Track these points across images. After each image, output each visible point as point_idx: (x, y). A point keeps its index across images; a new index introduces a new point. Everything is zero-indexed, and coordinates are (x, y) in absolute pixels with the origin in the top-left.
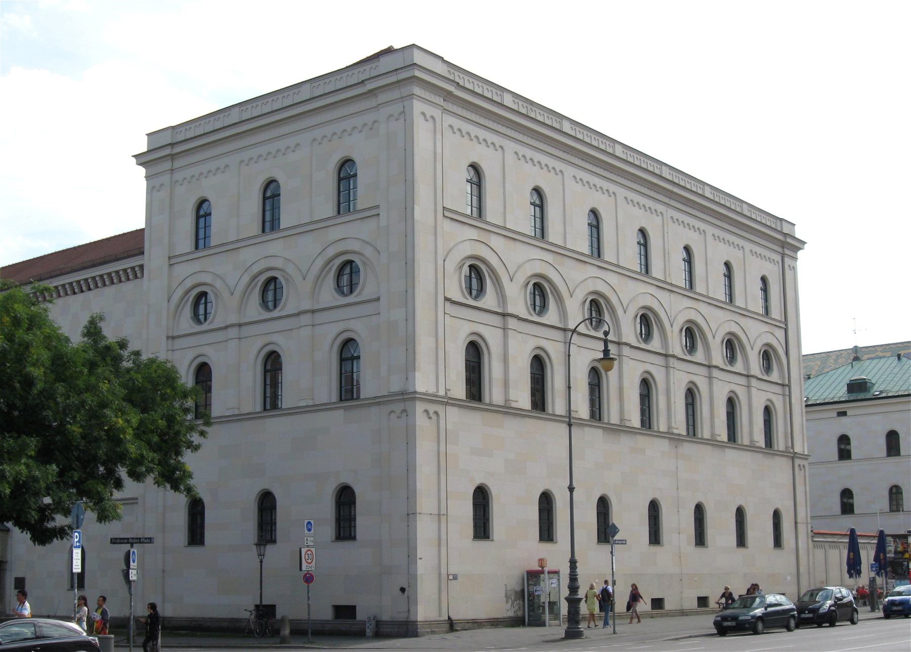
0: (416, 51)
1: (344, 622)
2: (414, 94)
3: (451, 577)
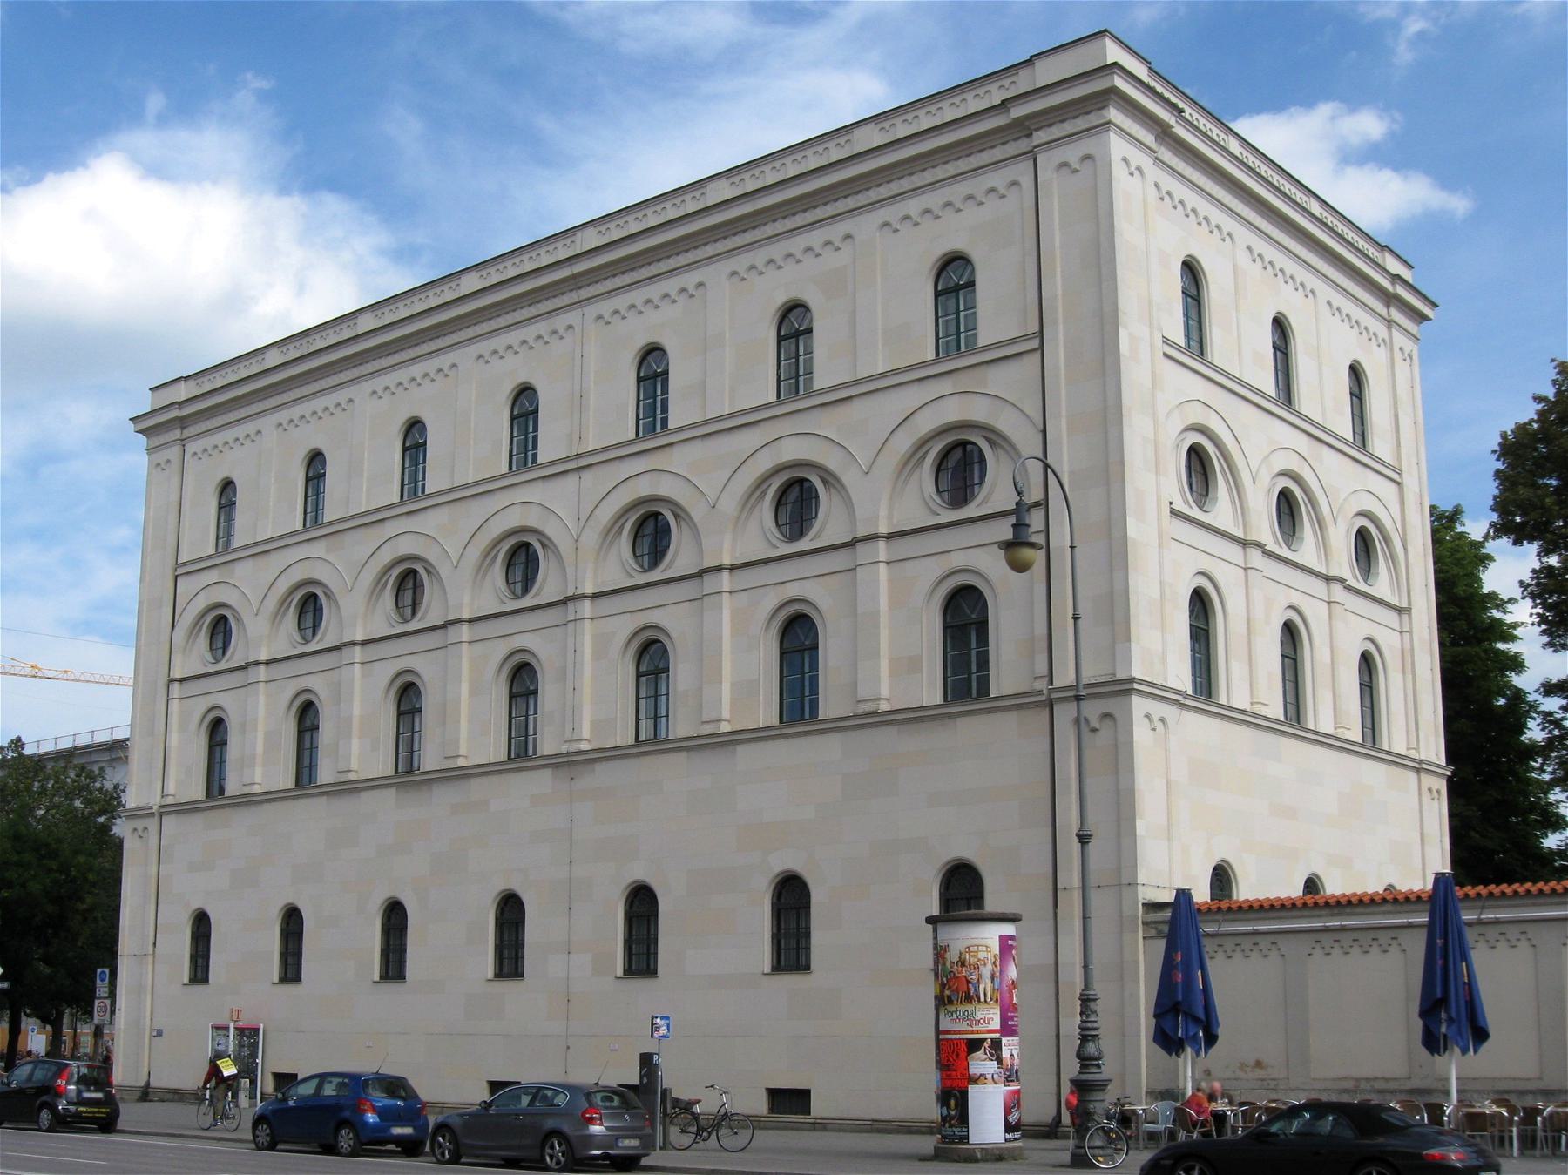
1: (802, 1120)
2: (1109, 122)
3: (155, 1033)
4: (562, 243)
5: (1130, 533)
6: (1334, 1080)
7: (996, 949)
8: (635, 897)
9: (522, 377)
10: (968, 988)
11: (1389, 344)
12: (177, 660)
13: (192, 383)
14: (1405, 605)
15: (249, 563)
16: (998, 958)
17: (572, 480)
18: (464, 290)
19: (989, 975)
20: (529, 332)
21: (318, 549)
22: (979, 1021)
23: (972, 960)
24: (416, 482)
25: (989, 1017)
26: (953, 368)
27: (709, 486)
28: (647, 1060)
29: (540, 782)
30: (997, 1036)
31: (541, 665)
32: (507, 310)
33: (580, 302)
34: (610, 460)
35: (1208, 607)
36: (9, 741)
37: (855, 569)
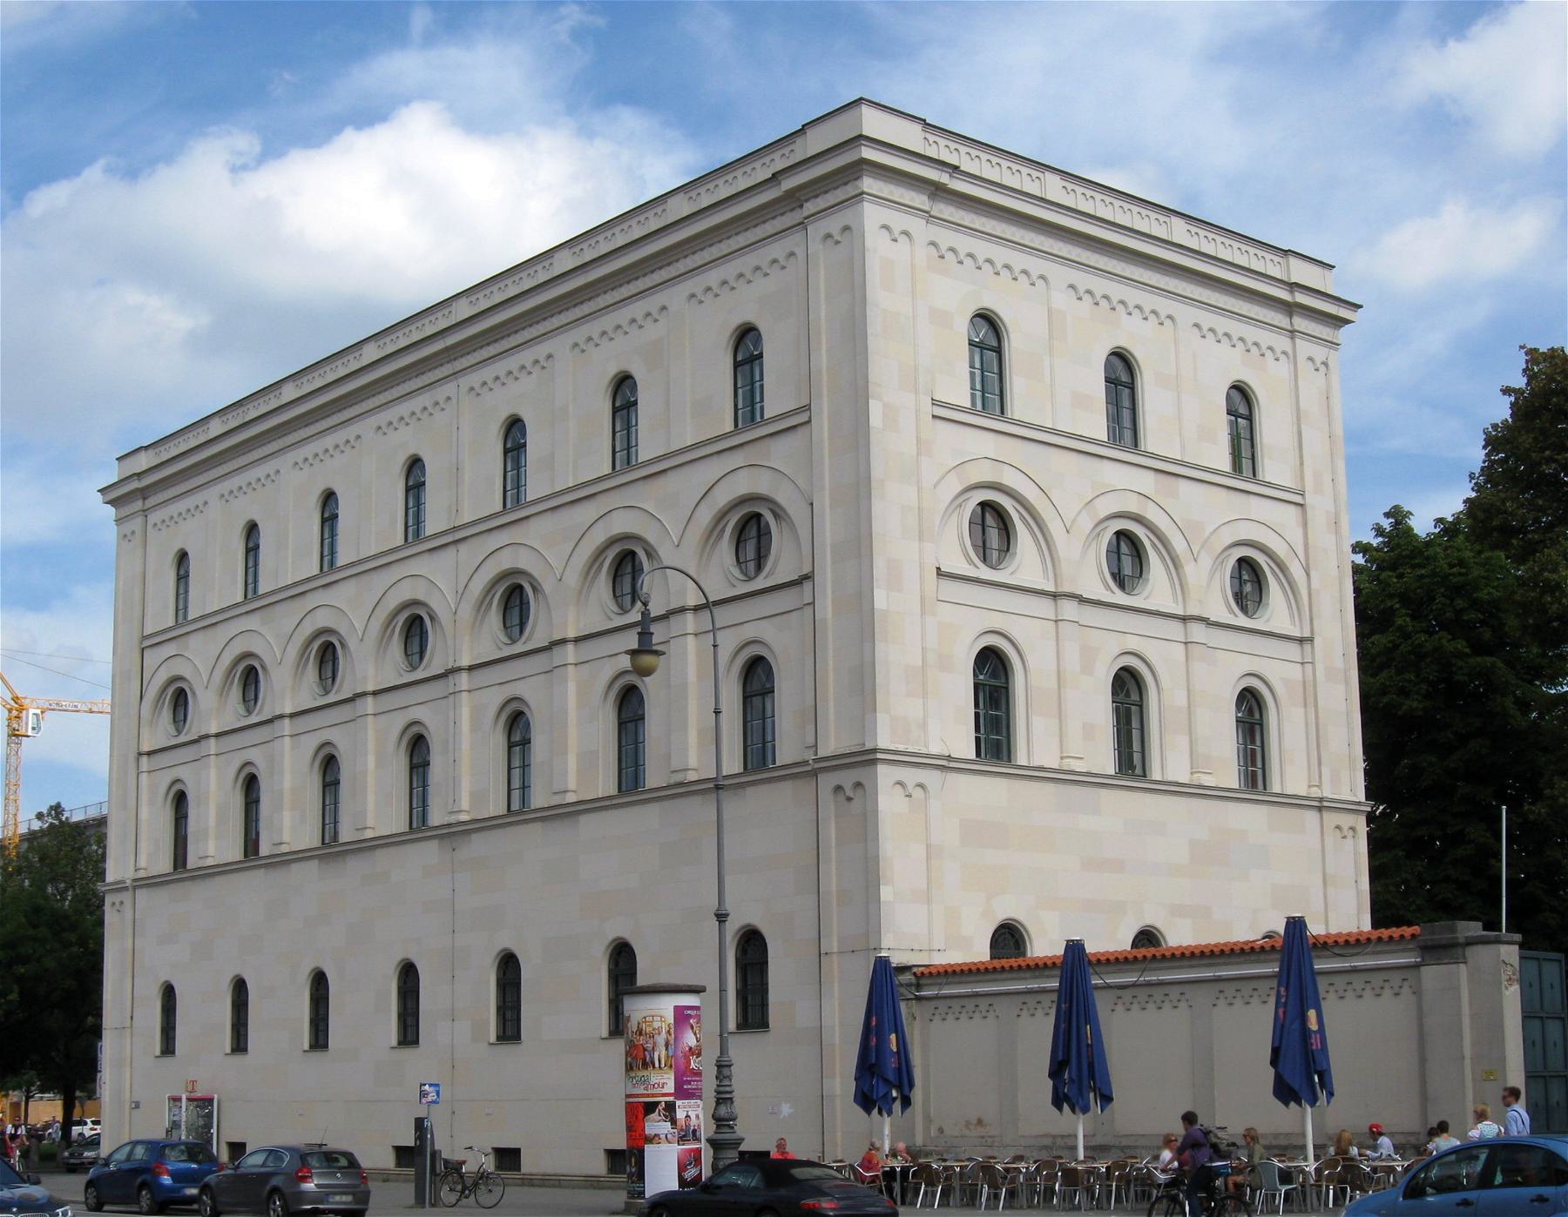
0: (865, 109)
2: (863, 193)
3: (133, 1106)
4: (780, 153)
5: (877, 605)
6: (1036, 1137)
7: (671, 1020)
8: (407, 976)
9: (412, 450)
10: (644, 1054)
11: (1292, 358)
12: (145, 732)
13: (151, 452)
14: (1307, 634)
15: (199, 636)
16: (672, 1027)
17: (451, 551)
18: (365, 361)
19: (663, 1043)
20: (415, 404)
21: (252, 622)
22: (654, 1085)
23: (648, 1030)
24: (753, 404)
25: (665, 1082)
26: (666, 467)
27: (555, 558)
28: (420, 1124)
29: (429, 852)
30: (671, 1099)
31: (646, 686)
32: (392, 384)
33: (455, 374)
34: (540, 512)
35: (1008, 668)
36: (48, 807)
37: (669, 641)
